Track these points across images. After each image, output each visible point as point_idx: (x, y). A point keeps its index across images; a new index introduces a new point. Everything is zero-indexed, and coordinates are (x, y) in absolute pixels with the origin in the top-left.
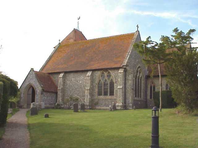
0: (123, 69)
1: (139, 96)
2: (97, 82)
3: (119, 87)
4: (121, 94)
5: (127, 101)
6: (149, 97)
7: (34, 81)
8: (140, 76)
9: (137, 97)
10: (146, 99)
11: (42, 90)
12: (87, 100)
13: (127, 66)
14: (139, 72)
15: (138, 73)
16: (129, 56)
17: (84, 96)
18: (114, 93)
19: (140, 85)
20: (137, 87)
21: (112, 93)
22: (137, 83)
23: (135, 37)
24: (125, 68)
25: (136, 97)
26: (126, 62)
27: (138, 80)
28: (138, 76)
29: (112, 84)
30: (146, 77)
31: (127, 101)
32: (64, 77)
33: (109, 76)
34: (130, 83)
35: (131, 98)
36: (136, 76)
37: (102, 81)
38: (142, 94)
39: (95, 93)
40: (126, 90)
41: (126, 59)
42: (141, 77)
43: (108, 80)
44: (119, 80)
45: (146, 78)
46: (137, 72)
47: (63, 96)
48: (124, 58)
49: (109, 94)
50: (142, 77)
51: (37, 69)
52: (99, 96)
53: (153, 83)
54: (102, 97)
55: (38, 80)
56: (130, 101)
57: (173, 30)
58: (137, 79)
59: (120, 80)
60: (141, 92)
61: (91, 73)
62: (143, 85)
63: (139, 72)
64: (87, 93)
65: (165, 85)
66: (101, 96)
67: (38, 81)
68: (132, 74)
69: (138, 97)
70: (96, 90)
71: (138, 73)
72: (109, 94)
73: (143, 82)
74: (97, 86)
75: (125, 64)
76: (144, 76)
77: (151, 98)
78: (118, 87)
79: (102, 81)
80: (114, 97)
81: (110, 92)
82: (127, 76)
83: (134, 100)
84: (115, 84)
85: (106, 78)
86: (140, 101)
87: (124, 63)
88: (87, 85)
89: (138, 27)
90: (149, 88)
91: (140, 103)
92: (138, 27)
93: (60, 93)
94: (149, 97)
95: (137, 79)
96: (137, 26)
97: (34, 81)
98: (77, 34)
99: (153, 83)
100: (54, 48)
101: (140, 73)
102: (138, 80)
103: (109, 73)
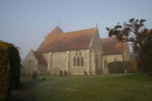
0: (90, 49)
2: (73, 57)
3: (87, 61)
4: (89, 65)
5: (92, 69)
6: (103, 67)
7: (33, 57)
9: (63, 72)
11: (38, 63)
12: (88, 65)
15: (98, 52)
16: (92, 42)
17: (64, 66)
18: (84, 65)
21: (82, 65)
23: (96, 30)
24: (90, 49)
27: (98, 55)
29: (82, 58)
32: (51, 55)
33: (80, 54)
34: (93, 59)
35: (94, 67)
36: (97, 54)
37: (76, 58)
38: (100, 65)
39: (71, 64)
40: (92, 63)
43: (80, 57)
44: (87, 56)
47: (51, 67)
48: (89, 43)
49: (80, 65)
51: (35, 50)
52: (74, 67)
54: (76, 67)
55: (35, 56)
57: (129, 20)
59: (88, 56)
61: (69, 52)
64: (67, 64)
66: (75, 67)
67: (36, 57)
70: (72, 63)
72: (80, 65)
74: (73, 60)
75: (91, 46)
78: (86, 60)
79: (76, 58)
80: (84, 67)
81: (81, 64)
82: (92, 54)
84: (84, 59)
85: (79, 55)
87: (90, 46)
88: (66, 59)
89: (97, 24)
92: (97, 24)
93: (49, 64)
94: (103, 67)
97: (33, 57)
98: (58, 30)
100: (45, 38)
101: (98, 52)
102: (98, 55)
103: (80, 52)
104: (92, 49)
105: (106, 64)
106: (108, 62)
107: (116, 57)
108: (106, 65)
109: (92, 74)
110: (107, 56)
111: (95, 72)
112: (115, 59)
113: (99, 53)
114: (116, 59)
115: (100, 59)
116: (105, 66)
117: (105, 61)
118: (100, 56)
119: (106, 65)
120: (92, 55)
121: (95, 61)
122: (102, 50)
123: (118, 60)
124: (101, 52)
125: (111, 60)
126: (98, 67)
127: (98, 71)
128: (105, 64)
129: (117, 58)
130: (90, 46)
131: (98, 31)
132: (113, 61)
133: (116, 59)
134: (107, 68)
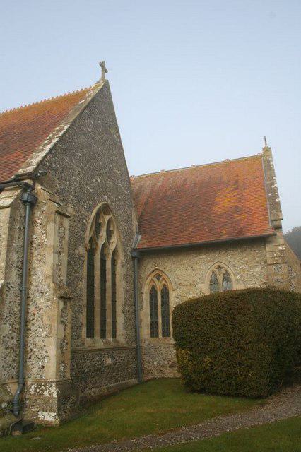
1: (109, 328)
5: (33, 367)
6: (145, 332)
8: (112, 247)
10: (137, 338)
13: (33, 176)
14: (104, 228)
15: (103, 233)
19: (109, 302)
20: (97, 291)
22: (97, 273)
25: (90, 334)
26: (36, 159)
27: (103, 262)
28: (100, 243)
30: (135, 254)
31: (35, 371)
35: (52, 351)
38: (120, 320)
40: (32, 308)
41: (42, 150)
42: (115, 252)
45: (134, 258)
46: (97, 227)
48: (32, 149)
50: (120, 253)
53: (158, 277)
56: (51, 372)
58: (98, 257)
60: (114, 312)
62: (121, 285)
63: (104, 228)
65: (207, 279)
68: (66, 222)
69: (103, 336)
71: (103, 233)
73: (120, 271)
75: (30, 169)
76: (125, 251)
77: (154, 333)
82: (38, 230)
83: (76, 354)
86: (111, 351)
89: (105, 70)
90: (144, 296)
91: (109, 361)
92: (105, 70)
94: (145, 332)
95: (98, 257)
96: (102, 65)
99: (158, 277)
104: (38, 187)
105: (165, 315)
106: (174, 301)
107: (219, 267)
108: (160, 320)
109: (28, 415)
110: (166, 259)
111: (52, 392)
112: (214, 281)
113: (114, 239)
114: (220, 278)
115: (119, 277)
116: (154, 325)
117: (153, 293)
118: (121, 260)
119: (160, 320)
120: (39, 236)
121: (58, 286)
122: (135, 229)
123: (238, 286)
124: (127, 236)
125: (193, 284)
126: (114, 336)
127: (109, 361)
128: (153, 313)
129: (227, 273)
130: (28, 165)
131: (109, 89)
132: (203, 289)
133: (220, 278)
134: (166, 334)
